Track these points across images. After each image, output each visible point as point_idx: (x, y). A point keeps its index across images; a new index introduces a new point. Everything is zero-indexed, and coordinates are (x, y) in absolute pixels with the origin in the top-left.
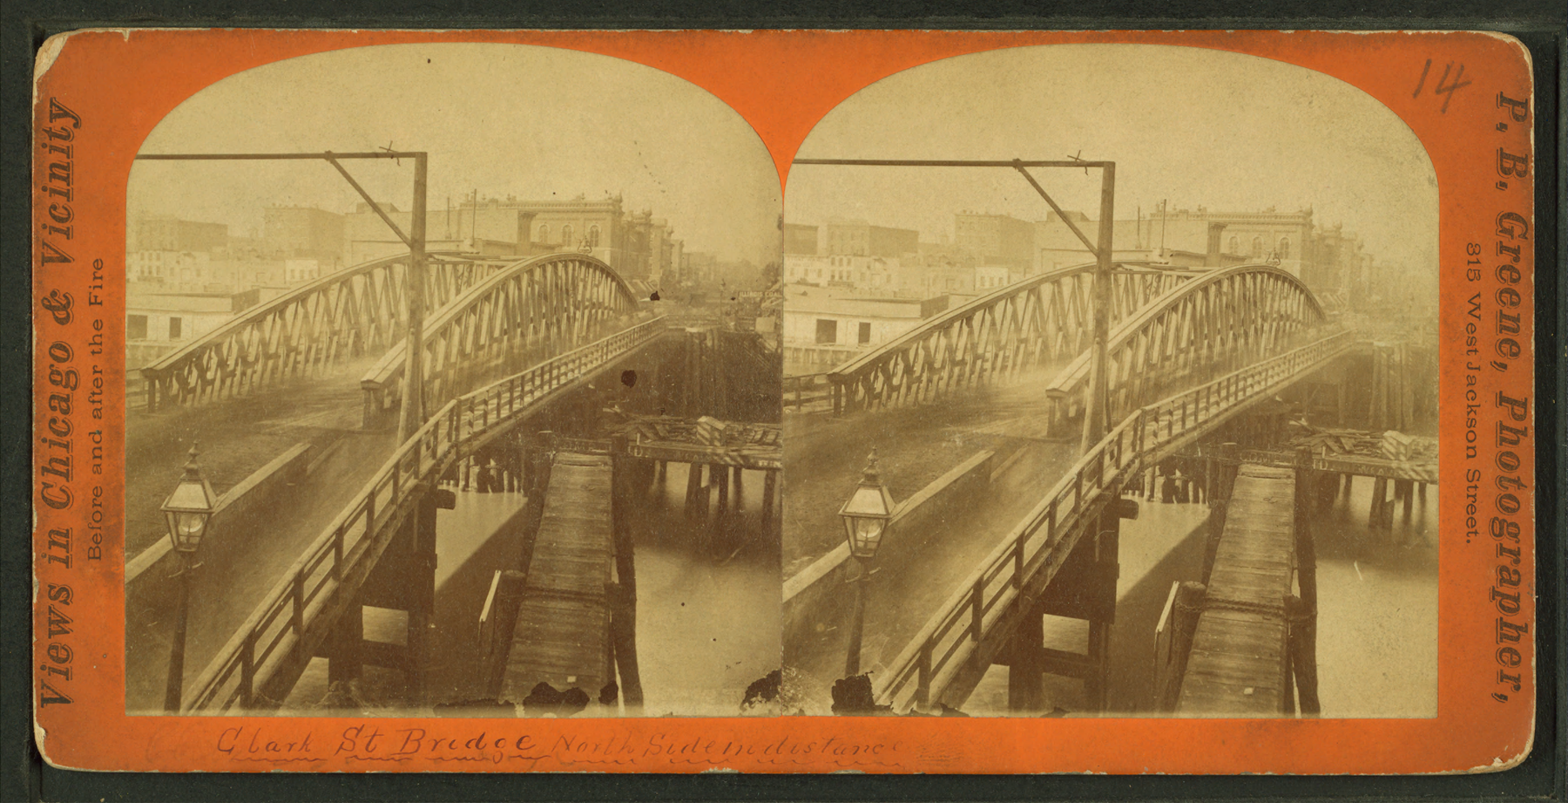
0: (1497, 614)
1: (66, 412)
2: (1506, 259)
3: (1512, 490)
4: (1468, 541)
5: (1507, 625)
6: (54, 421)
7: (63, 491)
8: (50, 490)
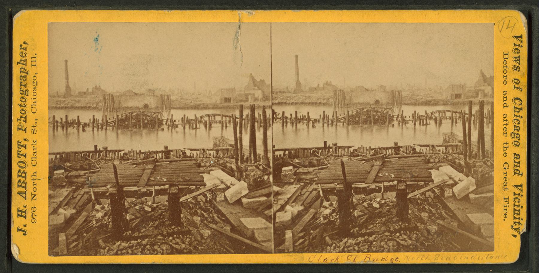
0: (26, 68)
1: (515, 126)
2: (23, 151)
3: (23, 104)
4: (36, 54)
5: (24, 64)
6: (519, 123)
7: (516, 103)
8: (520, 103)
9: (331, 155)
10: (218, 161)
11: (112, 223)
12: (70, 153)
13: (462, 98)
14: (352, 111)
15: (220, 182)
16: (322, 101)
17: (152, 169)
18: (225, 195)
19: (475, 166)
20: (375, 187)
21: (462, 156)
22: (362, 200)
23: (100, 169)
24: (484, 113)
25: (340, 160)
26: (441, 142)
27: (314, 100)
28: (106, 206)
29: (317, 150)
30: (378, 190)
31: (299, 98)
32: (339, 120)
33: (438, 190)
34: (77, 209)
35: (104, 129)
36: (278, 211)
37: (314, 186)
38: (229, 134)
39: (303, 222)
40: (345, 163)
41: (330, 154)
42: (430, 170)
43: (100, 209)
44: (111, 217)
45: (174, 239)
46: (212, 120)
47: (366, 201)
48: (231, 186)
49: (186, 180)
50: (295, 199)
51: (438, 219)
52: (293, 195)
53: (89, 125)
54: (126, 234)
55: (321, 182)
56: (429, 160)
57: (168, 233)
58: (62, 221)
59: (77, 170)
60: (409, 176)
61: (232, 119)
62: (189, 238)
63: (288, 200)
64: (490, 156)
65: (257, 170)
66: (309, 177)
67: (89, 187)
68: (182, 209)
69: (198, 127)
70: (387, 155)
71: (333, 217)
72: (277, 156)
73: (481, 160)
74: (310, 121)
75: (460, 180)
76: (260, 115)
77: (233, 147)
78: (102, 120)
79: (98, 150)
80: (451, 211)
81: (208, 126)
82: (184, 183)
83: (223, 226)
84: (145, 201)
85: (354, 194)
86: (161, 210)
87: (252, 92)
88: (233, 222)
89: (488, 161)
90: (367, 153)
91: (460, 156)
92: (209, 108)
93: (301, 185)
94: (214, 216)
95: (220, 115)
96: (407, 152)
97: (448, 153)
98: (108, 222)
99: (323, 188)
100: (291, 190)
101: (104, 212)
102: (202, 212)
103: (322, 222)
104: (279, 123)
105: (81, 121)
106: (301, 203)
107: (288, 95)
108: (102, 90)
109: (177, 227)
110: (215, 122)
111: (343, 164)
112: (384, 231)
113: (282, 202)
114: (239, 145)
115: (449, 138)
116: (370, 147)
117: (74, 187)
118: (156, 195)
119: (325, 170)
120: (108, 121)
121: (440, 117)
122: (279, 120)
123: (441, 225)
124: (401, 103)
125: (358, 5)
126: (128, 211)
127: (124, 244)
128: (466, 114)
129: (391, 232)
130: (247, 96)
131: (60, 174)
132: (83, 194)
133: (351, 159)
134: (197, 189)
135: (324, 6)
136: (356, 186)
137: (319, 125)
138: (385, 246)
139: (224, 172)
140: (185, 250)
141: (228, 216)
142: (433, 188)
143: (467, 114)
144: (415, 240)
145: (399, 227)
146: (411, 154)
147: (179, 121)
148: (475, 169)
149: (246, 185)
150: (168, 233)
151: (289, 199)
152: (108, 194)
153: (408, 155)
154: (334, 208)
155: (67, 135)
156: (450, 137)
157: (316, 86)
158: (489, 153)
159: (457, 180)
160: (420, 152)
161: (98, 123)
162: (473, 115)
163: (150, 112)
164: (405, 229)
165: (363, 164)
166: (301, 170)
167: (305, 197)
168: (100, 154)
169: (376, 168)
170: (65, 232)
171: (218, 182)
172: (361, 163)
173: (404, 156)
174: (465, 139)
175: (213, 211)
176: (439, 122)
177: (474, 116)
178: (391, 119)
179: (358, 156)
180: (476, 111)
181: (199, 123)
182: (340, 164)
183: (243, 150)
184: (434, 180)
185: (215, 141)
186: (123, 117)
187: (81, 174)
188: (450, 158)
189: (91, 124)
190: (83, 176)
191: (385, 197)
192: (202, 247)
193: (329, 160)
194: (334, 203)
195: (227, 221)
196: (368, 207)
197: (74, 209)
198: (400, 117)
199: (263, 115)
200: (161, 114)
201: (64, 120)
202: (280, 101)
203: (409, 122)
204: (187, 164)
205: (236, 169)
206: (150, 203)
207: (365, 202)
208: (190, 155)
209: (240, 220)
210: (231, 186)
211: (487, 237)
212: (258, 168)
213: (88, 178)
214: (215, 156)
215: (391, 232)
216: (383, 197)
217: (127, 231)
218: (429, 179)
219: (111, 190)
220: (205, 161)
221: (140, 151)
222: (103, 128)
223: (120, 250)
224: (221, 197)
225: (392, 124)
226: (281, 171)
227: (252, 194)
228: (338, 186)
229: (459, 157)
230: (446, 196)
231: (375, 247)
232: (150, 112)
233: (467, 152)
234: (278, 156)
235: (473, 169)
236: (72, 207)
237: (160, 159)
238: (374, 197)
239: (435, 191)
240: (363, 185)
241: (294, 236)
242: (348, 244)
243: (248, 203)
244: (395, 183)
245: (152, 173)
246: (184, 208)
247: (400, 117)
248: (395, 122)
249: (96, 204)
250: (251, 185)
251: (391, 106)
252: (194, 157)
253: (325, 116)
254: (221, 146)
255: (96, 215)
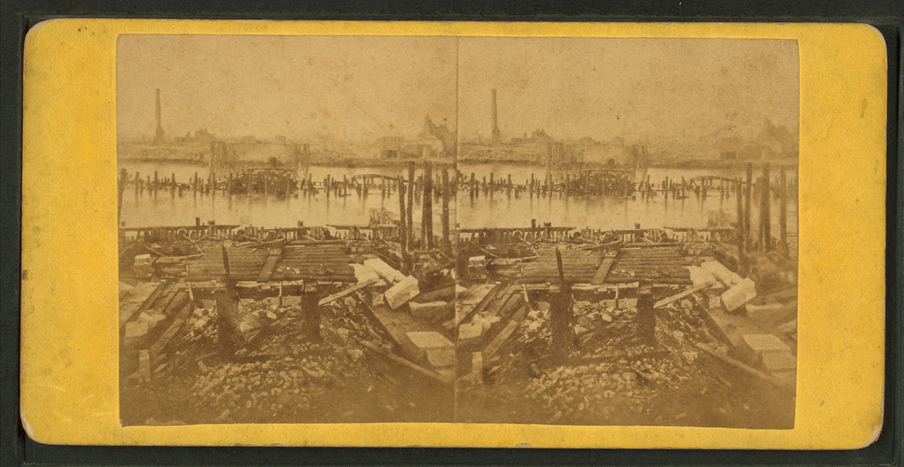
9: (207, 239)
10: (377, 245)
11: (219, 336)
12: (159, 229)
13: (399, 158)
14: (574, 175)
15: (715, 279)
16: (531, 159)
17: (615, 258)
18: (721, 299)
19: (417, 260)
20: (605, 290)
21: (398, 245)
22: (251, 307)
23: (203, 254)
24: (770, 183)
25: (554, 248)
26: (705, 226)
27: (181, 156)
28: (545, 313)
29: (521, 233)
30: (610, 295)
31: (496, 153)
32: (555, 187)
33: (363, 294)
34: (167, 314)
35: (210, 194)
36: (462, 322)
37: (516, 287)
38: (393, 205)
39: (500, 341)
40: (562, 253)
41: (204, 237)
42: (687, 267)
43: (200, 314)
44: (217, 327)
45: (643, 364)
46: (368, 184)
47: (257, 308)
48: (394, 283)
49: (665, 274)
50: (486, 306)
51: (363, 339)
52: (485, 298)
53: (525, 188)
54: (239, 353)
55: (527, 280)
56: (349, 249)
57: (300, 352)
58: (478, 334)
59: (169, 255)
60: (657, 275)
61: (397, 182)
62: (331, 360)
63: (143, 305)
64: (440, 245)
65: (433, 260)
66: (507, 272)
67: (520, 283)
68: (657, 319)
69: (348, 193)
70: (624, 243)
71: (208, 332)
72: (128, 238)
73: (426, 251)
74: (177, 186)
75: (395, 280)
76: (440, 177)
77: (399, 225)
78: (209, 181)
79: (201, 224)
80: (384, 328)
81: (362, 192)
82: (324, 277)
83: (717, 346)
84: (268, 303)
85: (575, 300)
86: (627, 319)
87: (428, 143)
88: (397, 339)
89: (437, 253)
90: (257, 236)
91: (396, 244)
92: (366, 166)
93: (497, 285)
94: (369, 328)
95: (718, 178)
96: (653, 239)
97: (378, 238)
98: (212, 334)
99: (194, 287)
100: (482, 291)
101: (207, 319)
102: (688, 324)
103: (526, 342)
104: (130, 189)
105: (177, 181)
106: (496, 313)
107: (480, 148)
108: (547, 136)
109: (314, 343)
110: (373, 186)
111: (558, 254)
112: (284, 354)
113: (468, 309)
114: (407, 221)
115: (379, 216)
116: (599, 230)
117: (164, 281)
118: (284, 294)
119: (532, 263)
120: (216, 181)
121: (365, 185)
122: (466, 186)
123: (369, 348)
124: (647, 164)
125: (611, 15)
126: (578, 321)
127: (236, 368)
128: (742, 183)
129: (629, 360)
130: (420, 148)
131: (143, 261)
132: (176, 291)
133: (570, 247)
134: (344, 287)
135: (554, 15)
136: (579, 288)
137: (188, 194)
138: (286, 377)
139: (385, 261)
140: (325, 379)
141: (389, 329)
142: (356, 292)
143: (744, 183)
144: (330, 369)
145: (641, 351)
146: (659, 241)
147: (320, 183)
148: (418, 264)
149: (416, 281)
150: (300, 352)
151: (145, 303)
152: (213, 292)
153: (319, 241)
154: (210, 317)
155: (156, 202)
156: (380, 215)
157: (184, 135)
158: (777, 243)
159: (391, 280)
160: (673, 239)
161: (202, 185)
162: (754, 185)
163: (616, 171)
164: (650, 355)
165: (589, 255)
166: (162, 260)
167: (167, 300)
168: (204, 231)
169: (608, 262)
170: (483, 351)
171: (374, 277)
172: (586, 254)
173: (649, 244)
174: (403, 218)
175: (368, 321)
176: (363, 192)
177: (416, 184)
178: (631, 190)
179: (581, 242)
180: (758, 179)
181: (349, 188)
182: (555, 253)
183: (413, 230)
184: (694, 281)
185: (372, 216)
186: (239, 177)
187: (175, 262)
188: (380, 247)
189: (528, 187)
190: (513, 265)
191: (621, 305)
192: (351, 375)
193: (538, 248)
194: (545, 313)
195: (387, 337)
196: (596, 320)
197: (497, 315)
198: (644, 185)
199: (443, 178)
200: (633, 175)
201: (488, 180)
202: (468, 157)
203: (320, 190)
204: (667, 252)
205: (402, 258)
206: (610, 310)
207: (256, 310)
208: (336, 236)
209: (406, 335)
210: (394, 283)
211: (435, 368)
212: (434, 256)
213: (185, 267)
214: (372, 237)
215: (629, 360)
216: (281, 303)
217: (239, 348)
218: (687, 281)
219: (218, 285)
220: (694, 247)
221: (262, 228)
222: (545, 194)
223: (562, 380)
224: (379, 300)
225: (633, 195)
226: (134, 261)
227: (426, 296)
228: (551, 288)
229: (393, 245)
230: (374, 304)
231: (604, 380)
232: (616, 171)
233: (406, 238)
234: (464, 240)
235: (414, 264)
236: (160, 310)
237: (628, 242)
238: (604, 306)
239: (357, 296)
240: (588, 287)
241: (151, 359)
242: (564, 376)
243: (418, 310)
244: (636, 284)
245: (278, 262)
246: (325, 315)
247: (644, 185)
248: (638, 193)
249: (531, 309)
250: (423, 282)
251: (632, 169)
252: (341, 238)
253: (197, 180)
254: (381, 222)
255: (530, 326)
